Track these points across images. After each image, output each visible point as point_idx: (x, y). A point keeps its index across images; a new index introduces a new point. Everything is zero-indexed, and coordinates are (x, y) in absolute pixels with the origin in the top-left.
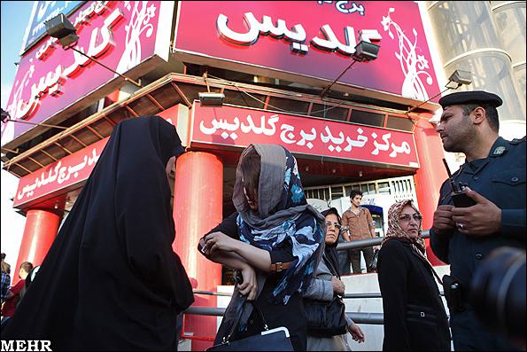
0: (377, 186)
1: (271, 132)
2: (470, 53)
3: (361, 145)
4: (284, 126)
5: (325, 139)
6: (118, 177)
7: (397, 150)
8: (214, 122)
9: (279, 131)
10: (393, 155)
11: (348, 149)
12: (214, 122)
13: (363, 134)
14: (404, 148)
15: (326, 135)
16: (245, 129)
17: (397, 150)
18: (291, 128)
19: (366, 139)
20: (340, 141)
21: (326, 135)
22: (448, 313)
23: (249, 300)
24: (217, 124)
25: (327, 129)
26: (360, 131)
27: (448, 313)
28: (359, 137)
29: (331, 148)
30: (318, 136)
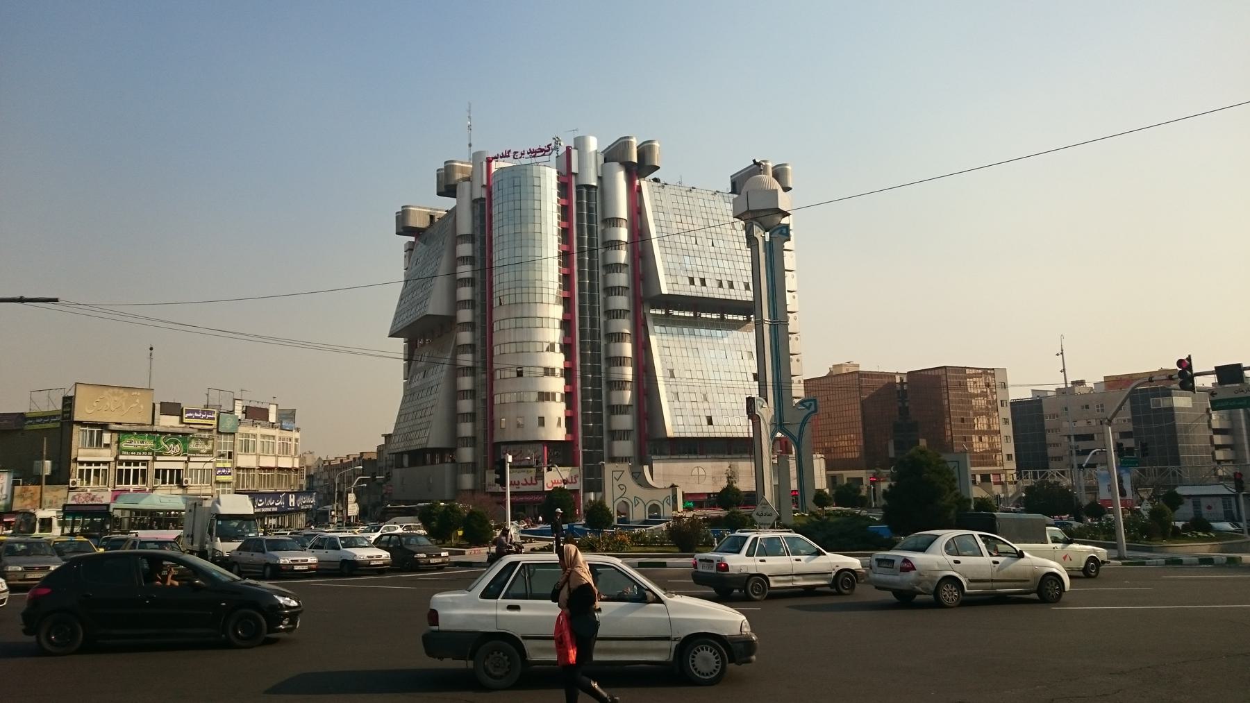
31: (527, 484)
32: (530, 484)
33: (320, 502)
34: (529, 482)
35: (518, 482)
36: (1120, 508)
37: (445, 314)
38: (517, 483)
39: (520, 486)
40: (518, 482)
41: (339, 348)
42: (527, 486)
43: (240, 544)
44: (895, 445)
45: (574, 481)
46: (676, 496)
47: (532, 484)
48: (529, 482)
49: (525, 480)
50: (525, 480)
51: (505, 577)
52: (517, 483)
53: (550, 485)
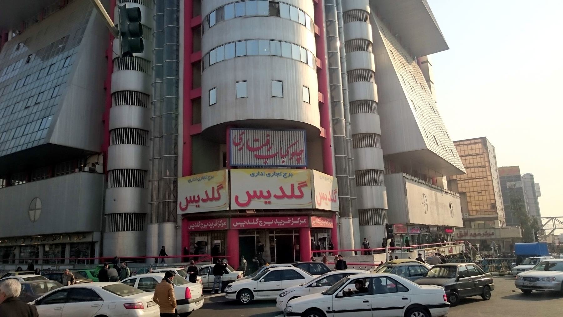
0: (497, 257)
1: (256, 223)
2: (191, 256)
3: (288, 222)
4: (260, 221)
5: (209, 225)
6: (505, 245)
7: (223, 225)
8: (237, 223)
9: (200, 225)
10: (300, 224)
11: (283, 224)
12: (237, 223)
13: (290, 219)
14: (305, 221)
15: (276, 221)
16: (247, 224)
17: (302, 222)
18: (262, 221)
19: (290, 221)
20: (281, 222)
21: (276, 221)
22: (256, 253)
23: (482, 297)
24: (237, 224)
25: (248, 220)
26: (289, 218)
27: (256, 253)
28: (289, 220)
29: (279, 225)
30: (274, 222)
31: (284, 196)
32: (289, 197)
33: (483, 268)
34: (288, 193)
35: (268, 192)
36: (310, 238)
37: (421, 57)
38: (265, 194)
39: (272, 199)
40: (268, 192)
41: (143, 180)
42: (286, 199)
43: (318, 34)
44: (395, 173)
45: (297, 193)
46: (360, 230)
47: (293, 196)
48: (288, 193)
49: (281, 189)
50: (281, 189)
51: (49, 298)
52: (265, 194)
53: (243, 199)
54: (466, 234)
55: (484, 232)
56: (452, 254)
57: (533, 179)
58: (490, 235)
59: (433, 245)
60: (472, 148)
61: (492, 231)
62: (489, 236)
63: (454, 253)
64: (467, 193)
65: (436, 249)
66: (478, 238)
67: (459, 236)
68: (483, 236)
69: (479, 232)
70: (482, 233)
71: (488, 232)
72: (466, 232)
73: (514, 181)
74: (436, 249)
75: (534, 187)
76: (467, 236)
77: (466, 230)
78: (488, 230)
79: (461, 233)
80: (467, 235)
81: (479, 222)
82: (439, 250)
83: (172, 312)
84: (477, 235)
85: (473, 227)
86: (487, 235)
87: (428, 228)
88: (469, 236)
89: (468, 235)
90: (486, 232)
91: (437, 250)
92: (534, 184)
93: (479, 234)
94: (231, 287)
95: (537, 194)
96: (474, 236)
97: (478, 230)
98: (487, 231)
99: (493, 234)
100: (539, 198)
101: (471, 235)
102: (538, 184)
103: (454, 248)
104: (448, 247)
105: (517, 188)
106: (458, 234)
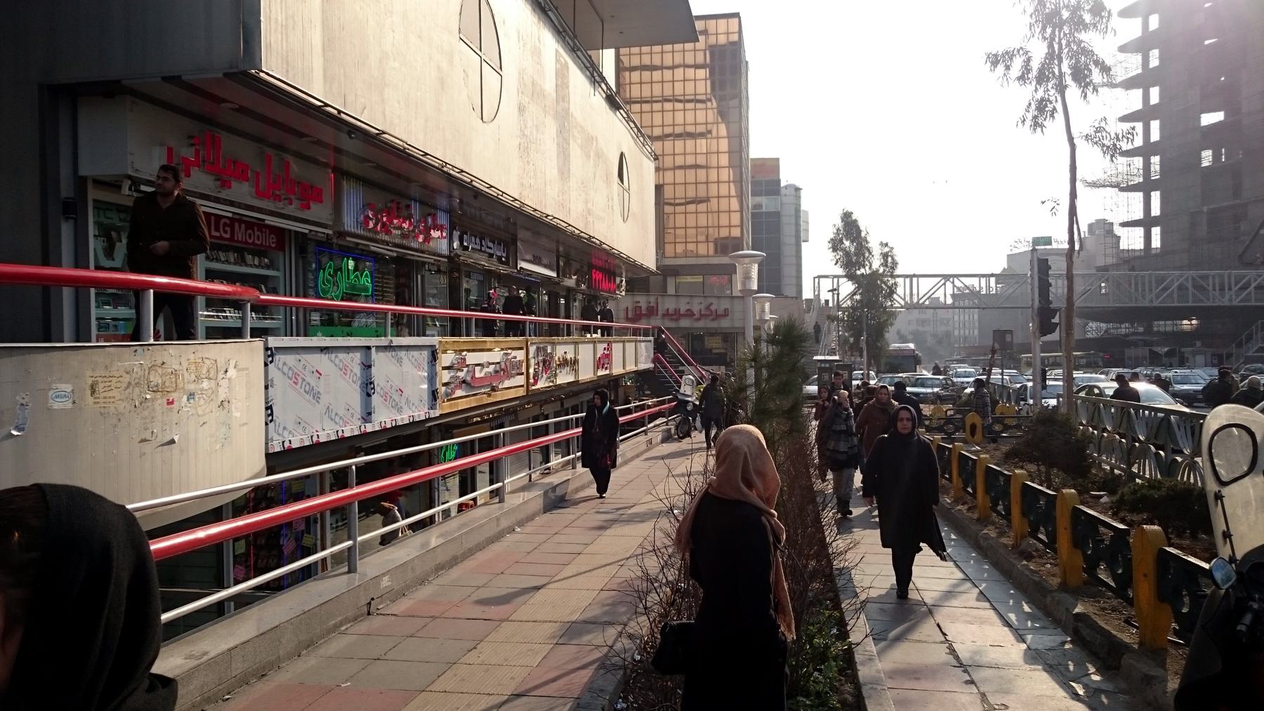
54: (652, 311)
55: (702, 307)
56: (607, 372)
57: (798, 198)
58: (717, 316)
59: (518, 322)
60: (687, 77)
61: (724, 304)
62: (713, 320)
63: (617, 370)
64: (665, 187)
65: (532, 349)
66: (685, 323)
67: (630, 315)
68: (698, 320)
69: (688, 307)
70: (696, 309)
71: (713, 308)
72: (652, 305)
73: (766, 195)
74: (532, 349)
75: (800, 217)
76: (653, 317)
77: (652, 299)
78: (714, 301)
79: (637, 309)
80: (653, 314)
81: (689, 279)
82: (546, 354)
83: (424, 389)
84: (684, 315)
85: (671, 290)
86: (709, 315)
87: (512, 248)
88: (659, 317)
89: (657, 315)
90: (708, 308)
91: (538, 349)
92: (800, 211)
93: (690, 314)
94: (819, 323)
95: (802, 234)
96: (675, 317)
97: (687, 300)
98: (712, 304)
99: (726, 313)
100: (804, 245)
101: (667, 315)
102: (806, 213)
103: (617, 348)
104: (594, 342)
105: (769, 214)
106: (630, 308)
